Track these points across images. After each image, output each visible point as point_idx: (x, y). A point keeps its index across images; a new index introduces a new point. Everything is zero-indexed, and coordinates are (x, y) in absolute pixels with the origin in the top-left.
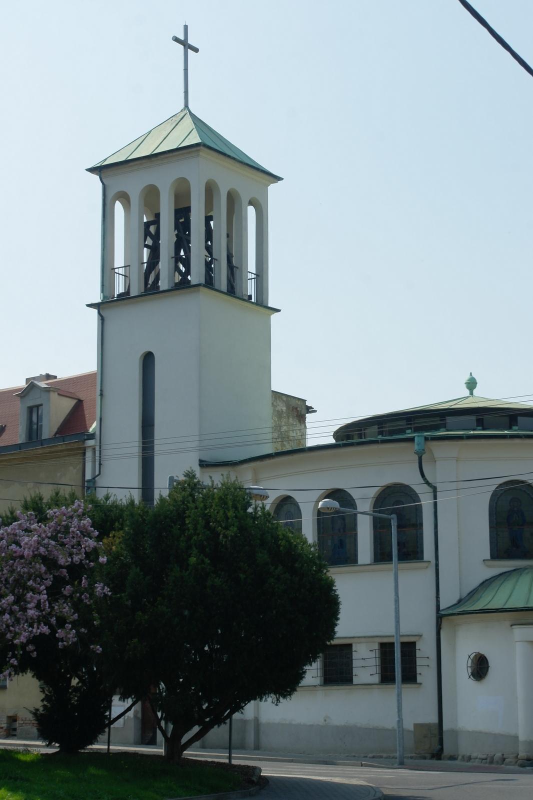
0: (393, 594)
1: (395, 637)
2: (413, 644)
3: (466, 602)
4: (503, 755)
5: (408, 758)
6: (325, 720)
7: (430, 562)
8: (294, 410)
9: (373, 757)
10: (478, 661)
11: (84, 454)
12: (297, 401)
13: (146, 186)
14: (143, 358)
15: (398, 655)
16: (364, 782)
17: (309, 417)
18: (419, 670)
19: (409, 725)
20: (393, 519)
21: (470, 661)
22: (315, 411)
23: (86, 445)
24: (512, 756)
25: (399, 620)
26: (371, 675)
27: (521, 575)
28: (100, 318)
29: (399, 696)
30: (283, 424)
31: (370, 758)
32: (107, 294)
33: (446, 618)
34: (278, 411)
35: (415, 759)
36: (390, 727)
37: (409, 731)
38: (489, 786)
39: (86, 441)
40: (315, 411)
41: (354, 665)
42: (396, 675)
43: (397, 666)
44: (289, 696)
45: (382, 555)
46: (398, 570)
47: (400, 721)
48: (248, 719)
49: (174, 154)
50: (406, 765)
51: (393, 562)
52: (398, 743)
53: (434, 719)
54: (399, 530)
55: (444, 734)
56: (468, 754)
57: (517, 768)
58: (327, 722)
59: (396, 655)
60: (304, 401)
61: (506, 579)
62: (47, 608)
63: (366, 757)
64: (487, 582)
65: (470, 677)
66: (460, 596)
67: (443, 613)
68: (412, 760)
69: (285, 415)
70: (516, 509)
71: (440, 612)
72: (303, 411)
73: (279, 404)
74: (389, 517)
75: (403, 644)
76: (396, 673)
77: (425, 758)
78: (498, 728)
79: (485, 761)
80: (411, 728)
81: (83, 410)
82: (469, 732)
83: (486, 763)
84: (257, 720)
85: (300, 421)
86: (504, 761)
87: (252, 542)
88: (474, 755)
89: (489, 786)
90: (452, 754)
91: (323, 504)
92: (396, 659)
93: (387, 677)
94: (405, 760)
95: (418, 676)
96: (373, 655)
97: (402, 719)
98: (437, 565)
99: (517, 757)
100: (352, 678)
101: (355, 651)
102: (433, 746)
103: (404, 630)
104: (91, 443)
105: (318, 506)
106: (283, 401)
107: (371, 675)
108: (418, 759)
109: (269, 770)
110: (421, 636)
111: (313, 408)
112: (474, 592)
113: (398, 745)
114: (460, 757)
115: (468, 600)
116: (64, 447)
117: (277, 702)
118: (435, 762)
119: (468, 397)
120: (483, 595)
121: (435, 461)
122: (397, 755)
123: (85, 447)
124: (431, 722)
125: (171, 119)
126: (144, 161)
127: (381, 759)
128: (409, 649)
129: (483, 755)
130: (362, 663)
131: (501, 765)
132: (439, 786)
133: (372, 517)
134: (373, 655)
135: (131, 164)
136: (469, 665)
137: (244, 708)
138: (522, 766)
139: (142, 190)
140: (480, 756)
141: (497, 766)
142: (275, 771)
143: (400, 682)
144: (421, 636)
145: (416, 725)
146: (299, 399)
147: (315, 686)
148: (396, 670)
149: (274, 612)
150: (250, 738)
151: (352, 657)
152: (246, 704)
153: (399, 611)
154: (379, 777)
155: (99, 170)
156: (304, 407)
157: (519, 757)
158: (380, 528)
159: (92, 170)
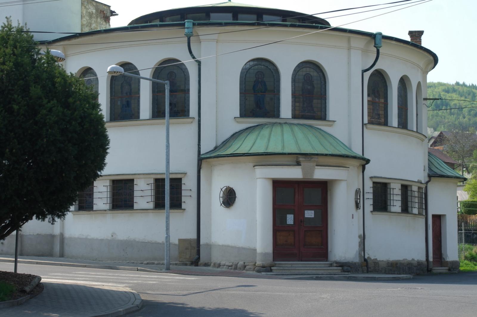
0: (165, 141)
1: (166, 174)
2: (180, 180)
3: (220, 149)
4: (244, 263)
5: (173, 264)
6: (112, 236)
7: (194, 118)
8: (102, 13)
9: (148, 264)
10: (228, 193)
12: (104, 7)
15: (167, 187)
16: (127, 288)
17: (112, 18)
18: (183, 199)
19: (174, 240)
20: (167, 84)
21: (222, 193)
22: (117, 15)
24: (251, 264)
25: (169, 161)
26: (147, 202)
27: (262, 129)
29: (168, 218)
30: (93, 22)
31: (145, 264)
33: (205, 160)
34: (89, 13)
35: (179, 265)
36: (161, 242)
37: (175, 245)
38: (233, 292)
40: (117, 15)
41: (135, 195)
42: (166, 203)
43: (167, 196)
44: (63, 216)
45: (158, 113)
46: (169, 124)
47: (168, 237)
48: (55, 234)
50: (172, 270)
51: (166, 118)
52: (165, 253)
53: (194, 236)
54: (172, 94)
55: (201, 247)
56: (219, 262)
57: (254, 273)
58: (113, 237)
59: (166, 187)
60: (109, 7)
61: (251, 131)
63: (142, 263)
64: (237, 134)
65: (221, 205)
66: (216, 144)
67: (203, 156)
68: (177, 266)
69: (94, 16)
70: (260, 80)
71: (200, 156)
72: (109, 14)
73: (90, 7)
74: (164, 82)
75: (172, 180)
76: (166, 201)
77: (186, 265)
78: (241, 243)
79: (231, 267)
80: (177, 242)
82: (219, 245)
83: (232, 269)
84: (62, 235)
85: (105, 21)
86: (245, 267)
87: (27, 78)
88: (223, 263)
89: (233, 292)
90: (206, 262)
91: (111, 69)
92: (166, 190)
93: (159, 205)
94: (171, 266)
95: (183, 203)
96: (149, 187)
97: (169, 235)
98: (199, 121)
99: (255, 265)
100: (133, 204)
101: (136, 184)
102: (193, 257)
103: (172, 169)
105: (107, 71)
106: (94, 5)
107: (147, 202)
108: (181, 265)
109: (59, 276)
110: (186, 174)
111: (116, 13)
112: (227, 141)
113: (165, 255)
114: (212, 264)
115: (222, 147)
117: (53, 222)
118: (194, 268)
119: (227, 2)
120: (233, 144)
121: (201, 42)
122: (165, 262)
124: (192, 238)
127: (154, 265)
128: (177, 183)
129: (230, 263)
130: (141, 194)
131: (243, 270)
132: (192, 292)
133: (151, 82)
134: (149, 187)
136: (221, 195)
137: (22, 226)
138: (259, 271)
140: (227, 264)
141: (240, 271)
142: (64, 276)
143: (169, 208)
144: (186, 174)
145: (180, 240)
146: (105, 5)
147: (105, 210)
148: (166, 199)
149: (45, 140)
150: (57, 248)
151: (133, 189)
152: (24, 223)
153: (169, 154)
154: (145, 282)
156: (109, 11)
157: (256, 264)
158: (157, 91)
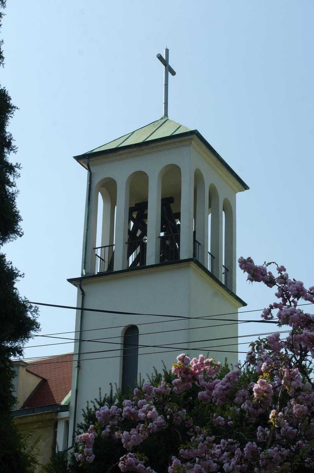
11: (56, 426)
13: (133, 173)
14: (124, 332)
23: (58, 417)
28: (81, 292)
32: (89, 271)
39: (60, 413)
49: (166, 142)
62: (301, 452)
81: (48, 388)
104: (64, 414)
116: (35, 418)
123: (57, 419)
125: (153, 123)
126: (134, 149)
135: (121, 152)
139: (131, 175)
155: (87, 157)
159: (78, 158)
